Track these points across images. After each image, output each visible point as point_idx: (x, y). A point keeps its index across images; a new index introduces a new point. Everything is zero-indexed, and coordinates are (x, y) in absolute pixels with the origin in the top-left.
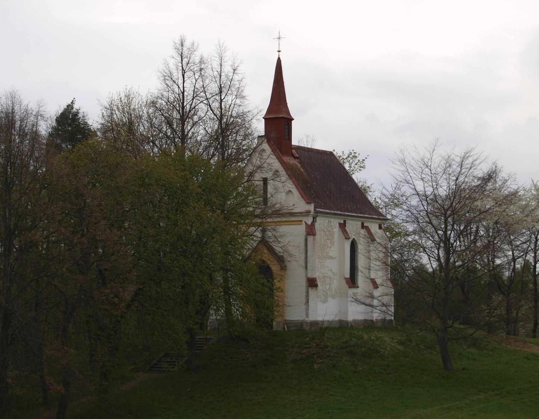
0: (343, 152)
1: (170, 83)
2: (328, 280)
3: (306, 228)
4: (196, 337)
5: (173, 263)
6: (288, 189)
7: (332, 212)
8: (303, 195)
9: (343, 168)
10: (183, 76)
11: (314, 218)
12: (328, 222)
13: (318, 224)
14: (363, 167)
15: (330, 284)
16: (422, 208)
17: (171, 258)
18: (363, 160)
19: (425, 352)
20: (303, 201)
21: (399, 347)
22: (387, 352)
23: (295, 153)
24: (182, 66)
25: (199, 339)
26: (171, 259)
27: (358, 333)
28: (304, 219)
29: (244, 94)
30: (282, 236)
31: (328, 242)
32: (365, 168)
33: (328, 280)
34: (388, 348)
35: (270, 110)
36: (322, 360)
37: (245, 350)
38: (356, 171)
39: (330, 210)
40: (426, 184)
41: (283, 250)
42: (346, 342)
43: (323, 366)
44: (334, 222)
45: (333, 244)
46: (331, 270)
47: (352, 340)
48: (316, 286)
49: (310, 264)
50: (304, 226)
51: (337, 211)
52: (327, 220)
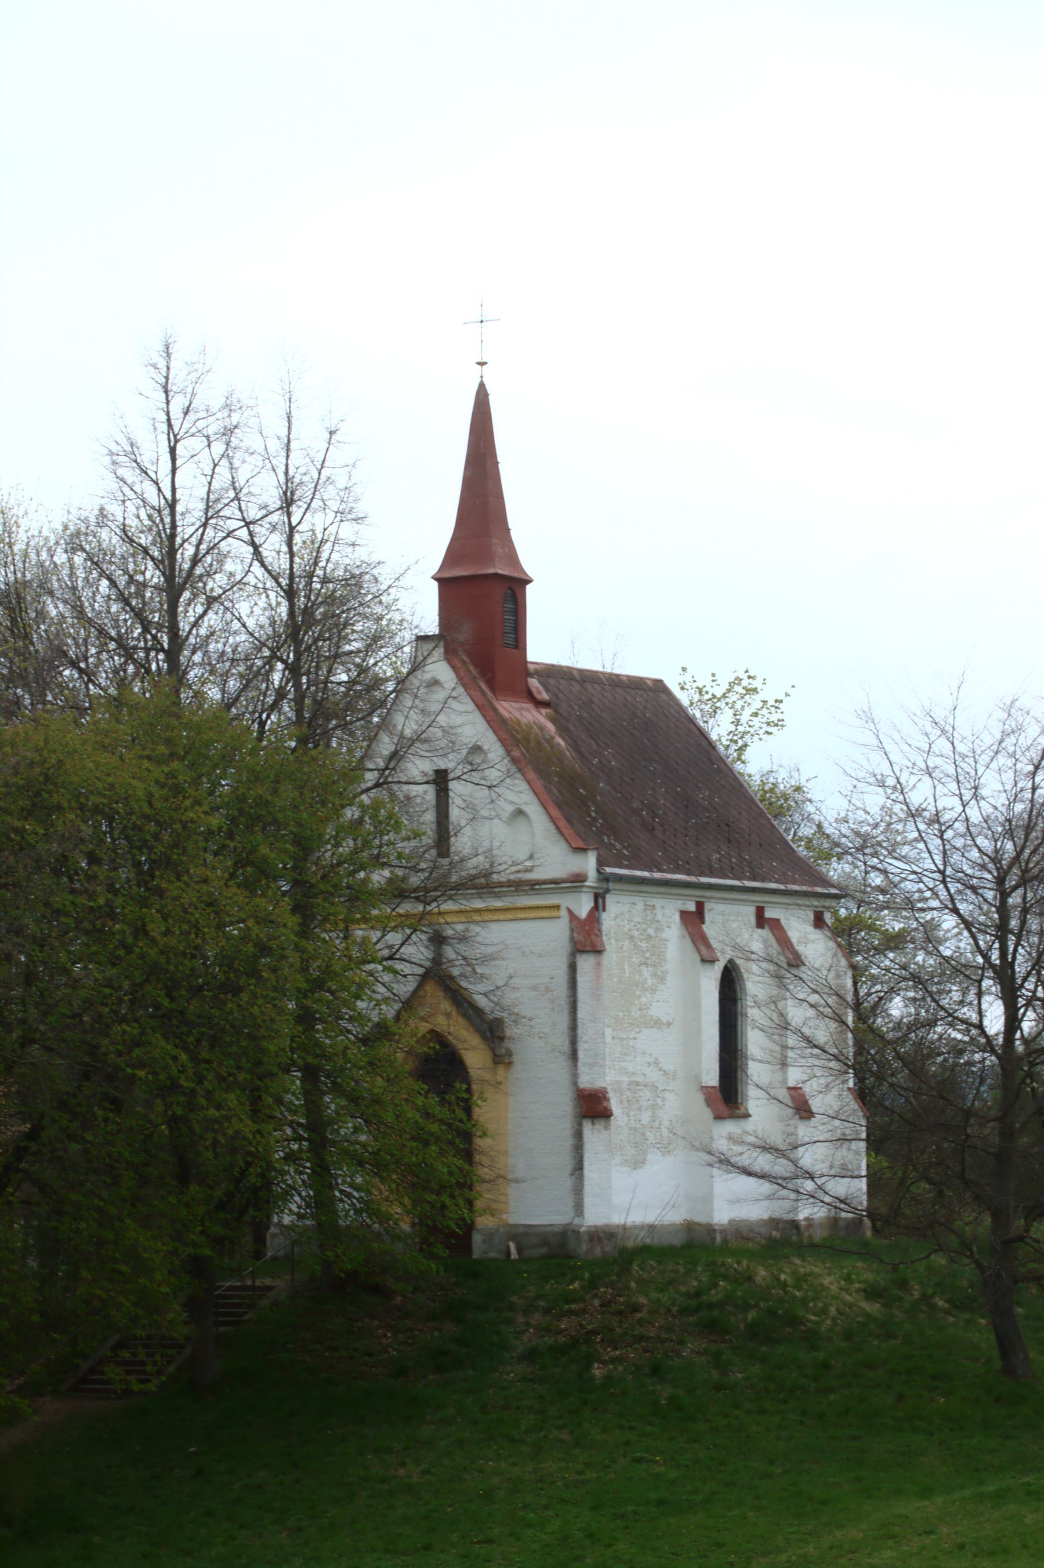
0: (713, 675)
1: (131, 475)
2: (648, 1093)
3: (572, 930)
4: (218, 1284)
5: (130, 1052)
6: (511, 808)
7: (657, 875)
8: (562, 824)
9: (697, 732)
10: (173, 451)
11: (596, 897)
12: (645, 910)
13: (612, 915)
14: (778, 724)
15: (654, 1107)
16: (929, 865)
17: (126, 1037)
18: (776, 701)
19: (951, 1319)
20: (563, 844)
21: (864, 1305)
22: (828, 1322)
23: (537, 688)
24: (169, 420)
25: (230, 1288)
26: (124, 1040)
27: (739, 1263)
28: (565, 901)
29: (361, 509)
30: (486, 959)
31: (646, 972)
32: (782, 726)
33: (646, 1094)
34: (833, 1310)
35: (453, 556)
36: (617, 1352)
37: (376, 1322)
38: (756, 738)
39: (650, 870)
40: (939, 787)
41: (493, 1002)
42: (698, 1294)
43: (620, 1368)
44: (663, 907)
45: (662, 980)
46: (656, 1062)
47: (715, 1285)
48: (605, 1115)
49: (586, 1046)
50: (564, 923)
51: (674, 873)
52: (640, 903)
